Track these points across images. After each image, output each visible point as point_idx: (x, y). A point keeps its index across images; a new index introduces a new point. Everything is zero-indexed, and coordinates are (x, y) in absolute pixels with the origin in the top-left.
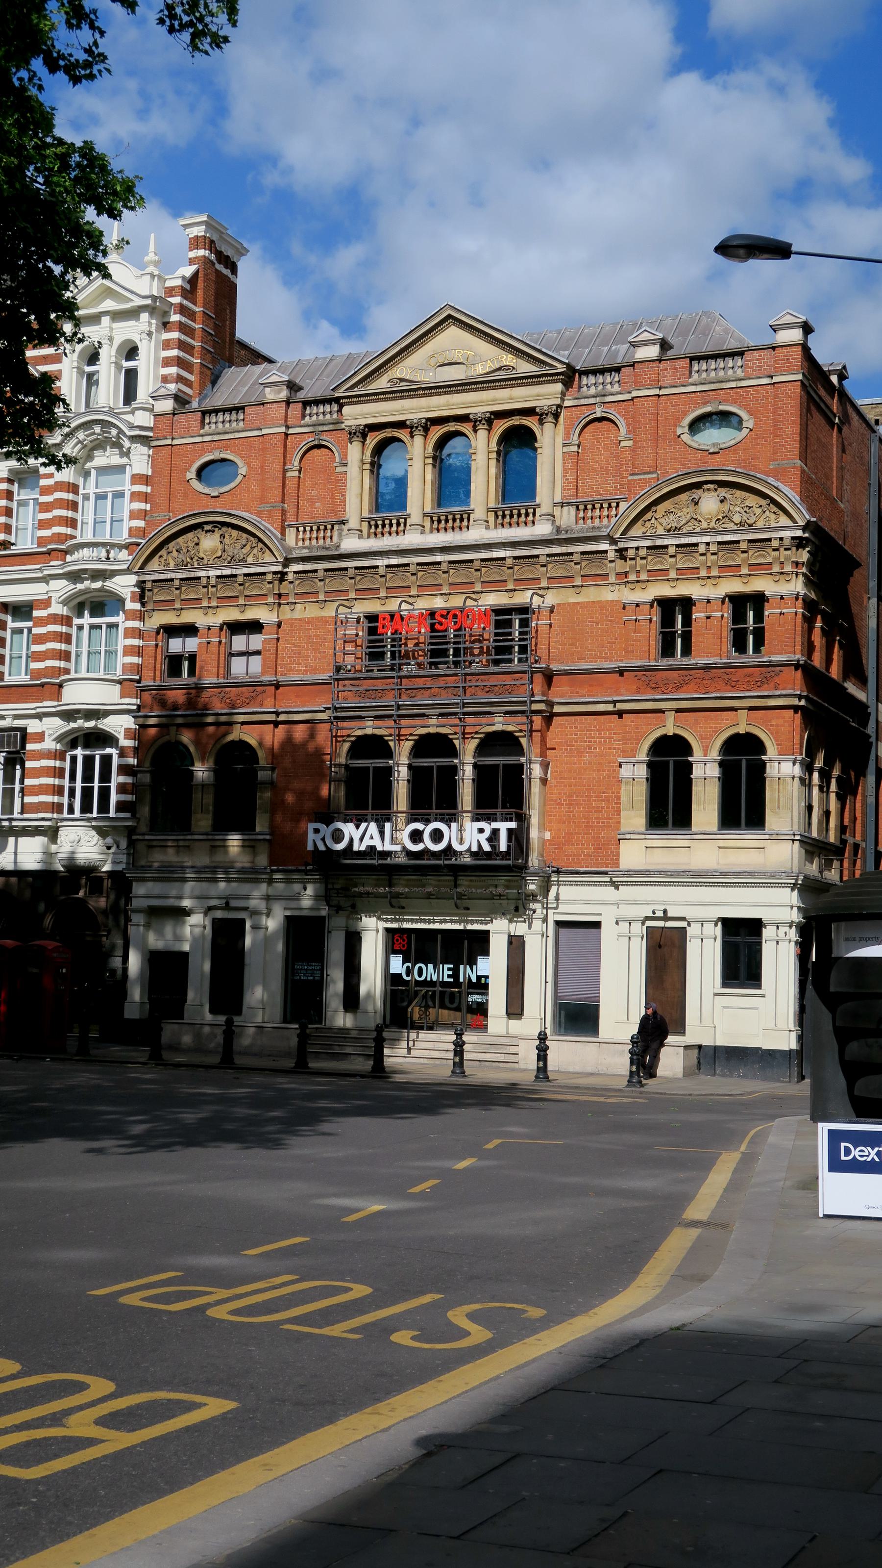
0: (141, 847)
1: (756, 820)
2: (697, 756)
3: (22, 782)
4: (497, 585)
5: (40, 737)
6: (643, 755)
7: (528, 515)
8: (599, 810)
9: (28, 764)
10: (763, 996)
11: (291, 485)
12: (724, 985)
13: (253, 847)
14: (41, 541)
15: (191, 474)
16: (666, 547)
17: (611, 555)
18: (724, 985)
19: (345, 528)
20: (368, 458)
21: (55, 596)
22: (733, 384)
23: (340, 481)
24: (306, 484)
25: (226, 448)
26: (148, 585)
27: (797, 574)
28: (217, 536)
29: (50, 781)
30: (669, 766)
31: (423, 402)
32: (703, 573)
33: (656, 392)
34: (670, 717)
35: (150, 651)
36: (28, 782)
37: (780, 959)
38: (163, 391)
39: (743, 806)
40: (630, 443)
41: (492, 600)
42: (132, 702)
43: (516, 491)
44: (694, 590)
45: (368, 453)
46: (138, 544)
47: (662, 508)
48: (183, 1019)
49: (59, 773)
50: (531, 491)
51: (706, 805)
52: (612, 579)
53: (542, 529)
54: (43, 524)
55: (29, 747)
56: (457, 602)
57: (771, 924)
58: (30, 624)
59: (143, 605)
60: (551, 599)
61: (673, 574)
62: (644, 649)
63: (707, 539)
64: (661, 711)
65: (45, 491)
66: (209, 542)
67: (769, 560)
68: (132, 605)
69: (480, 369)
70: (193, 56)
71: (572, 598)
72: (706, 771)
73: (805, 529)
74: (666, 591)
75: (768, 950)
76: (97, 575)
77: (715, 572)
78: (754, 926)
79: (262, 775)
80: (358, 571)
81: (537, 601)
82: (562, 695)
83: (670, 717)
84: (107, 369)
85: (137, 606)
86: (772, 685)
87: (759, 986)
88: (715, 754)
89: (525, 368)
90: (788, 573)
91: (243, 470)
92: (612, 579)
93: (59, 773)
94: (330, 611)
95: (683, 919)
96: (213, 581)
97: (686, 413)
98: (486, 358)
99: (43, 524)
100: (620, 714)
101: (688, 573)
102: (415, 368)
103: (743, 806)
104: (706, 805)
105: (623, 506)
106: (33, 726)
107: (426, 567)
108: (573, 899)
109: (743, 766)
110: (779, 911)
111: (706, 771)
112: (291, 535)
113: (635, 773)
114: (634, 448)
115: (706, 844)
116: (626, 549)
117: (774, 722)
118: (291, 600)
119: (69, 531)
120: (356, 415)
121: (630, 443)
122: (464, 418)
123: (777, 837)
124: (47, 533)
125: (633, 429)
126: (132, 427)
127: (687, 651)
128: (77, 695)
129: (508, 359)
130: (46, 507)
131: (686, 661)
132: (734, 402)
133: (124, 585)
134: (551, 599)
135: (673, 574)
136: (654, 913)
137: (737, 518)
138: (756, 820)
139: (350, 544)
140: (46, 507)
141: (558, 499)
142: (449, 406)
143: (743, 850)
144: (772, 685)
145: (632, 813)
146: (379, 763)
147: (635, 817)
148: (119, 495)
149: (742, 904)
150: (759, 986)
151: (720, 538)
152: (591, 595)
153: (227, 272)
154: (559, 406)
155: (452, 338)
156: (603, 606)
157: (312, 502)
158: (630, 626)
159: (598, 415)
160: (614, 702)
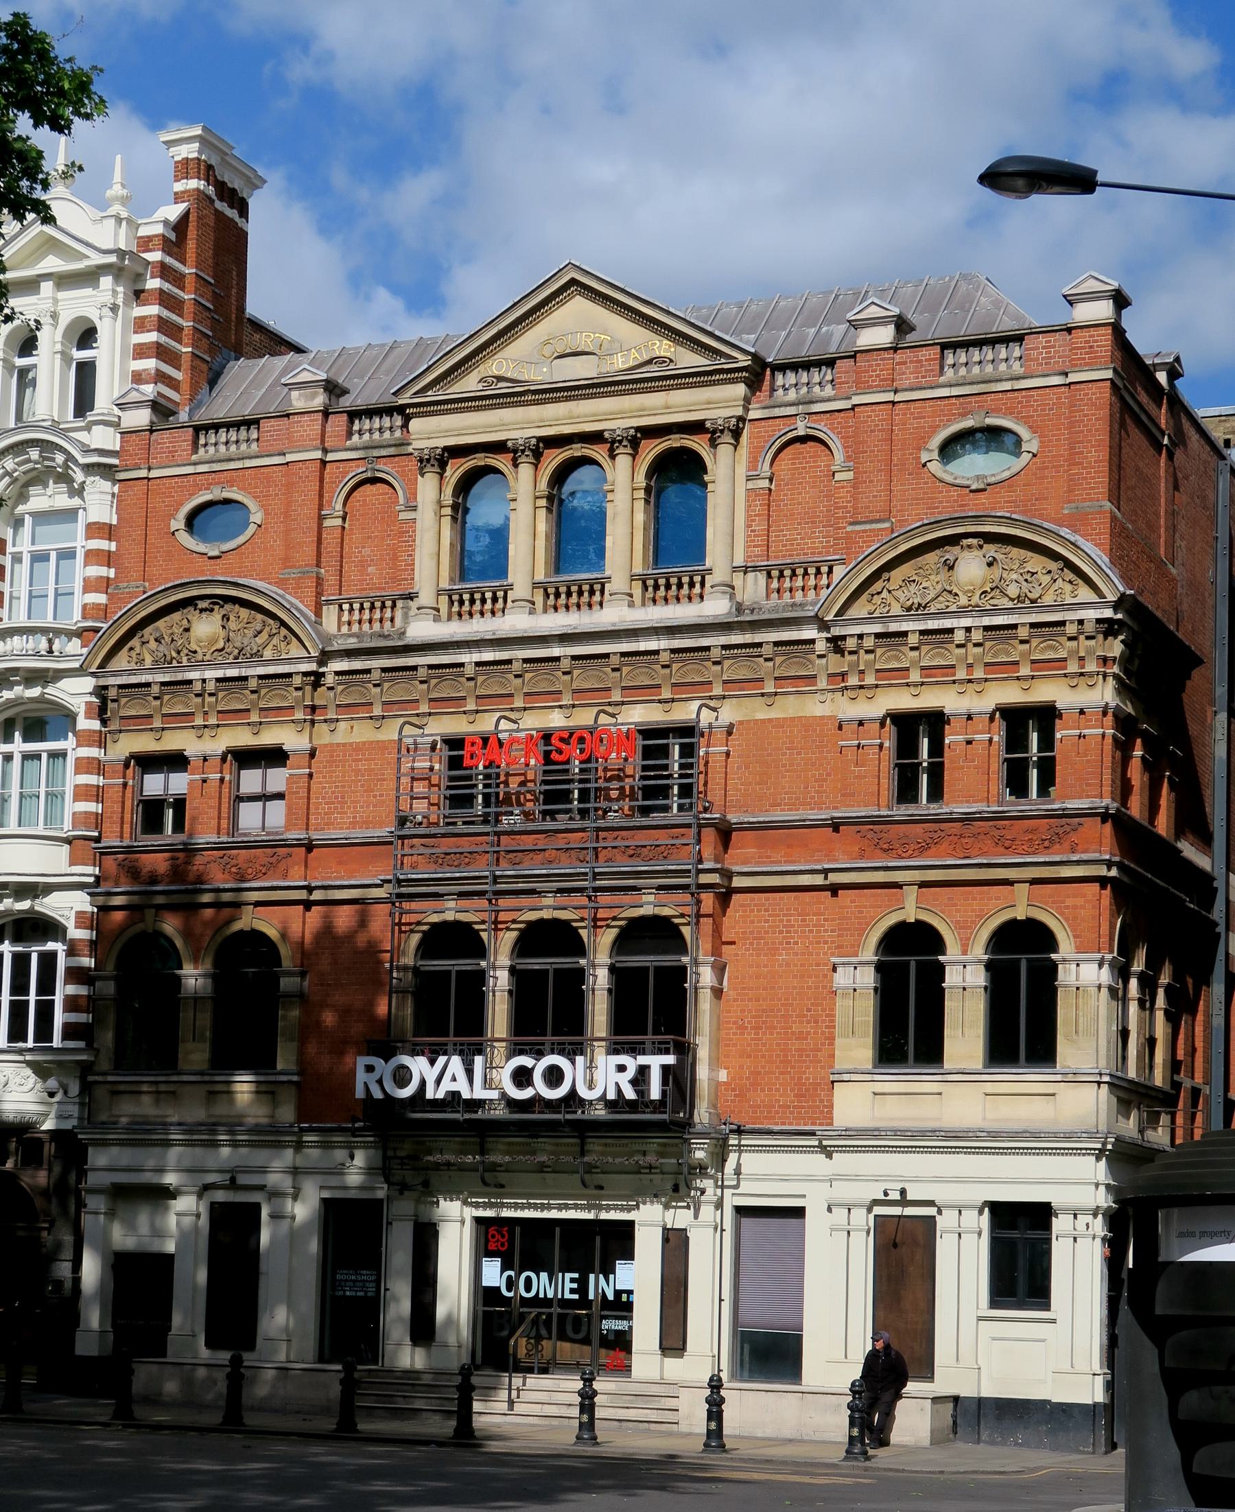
0: (100, 1093)
1: (1042, 1051)
2: (952, 953)
6: (869, 953)
8: (801, 1037)
10: (1053, 1321)
11: (330, 540)
12: (994, 1304)
13: (272, 1093)
15: (178, 523)
16: (904, 634)
17: (821, 646)
18: (994, 1304)
19: (413, 605)
22: (1007, 386)
23: (406, 533)
25: (231, 483)
26: (112, 693)
27: (1105, 676)
30: (909, 964)
31: (533, 412)
32: (961, 674)
33: (889, 397)
34: (911, 893)
35: (114, 794)
37: (1079, 1265)
38: (134, 397)
39: (1023, 1030)
40: (850, 475)
41: (639, 715)
43: (676, 548)
46: (96, 630)
48: (165, 1356)
52: (822, 683)
53: (715, 607)
57: (1066, 1211)
59: (104, 722)
60: (728, 713)
61: (915, 676)
62: (871, 792)
63: (967, 622)
66: (205, 627)
67: (1062, 654)
68: (87, 724)
69: (620, 362)
71: (759, 711)
72: (965, 978)
73: (1116, 606)
75: (1060, 1251)
77: (979, 673)
78: (1040, 1214)
79: (286, 983)
82: (745, 860)
83: (911, 893)
85: (96, 725)
86: (1066, 845)
87: (1047, 1307)
88: (979, 951)
89: (689, 360)
90: (1090, 674)
91: (257, 517)
92: (822, 683)
94: (390, 732)
95: (930, 1203)
96: (211, 686)
97: (934, 429)
98: (630, 345)
100: (834, 889)
101: (938, 675)
102: (520, 360)
103: (1023, 1030)
105: (839, 571)
107: (536, 664)
108: (763, 1173)
109: (1023, 963)
110: (1077, 1189)
111: (965, 978)
113: (857, 980)
114: (855, 483)
115: (965, 1088)
117: (1069, 902)
120: (430, 432)
121: (850, 475)
122: (595, 438)
123: (1074, 1078)
125: (854, 454)
126: (87, 451)
127: (936, 793)
129: (663, 347)
131: (934, 809)
132: (1009, 412)
133: (75, 693)
134: (728, 713)
135: (915, 676)
136: (886, 1194)
137: (1013, 591)
138: (1042, 1051)
139: (421, 629)
141: (739, 560)
143: (1022, 1097)
144: (1066, 845)
145: (853, 1041)
146: (465, 964)
147: (856, 1047)
148: (67, 555)
149: (1021, 1180)
150: (1047, 1307)
151: (987, 621)
152: (790, 707)
153: (232, 213)
154: (741, 419)
156: (808, 724)
157: (363, 565)
158: (850, 755)
159: (801, 432)
160: (826, 872)
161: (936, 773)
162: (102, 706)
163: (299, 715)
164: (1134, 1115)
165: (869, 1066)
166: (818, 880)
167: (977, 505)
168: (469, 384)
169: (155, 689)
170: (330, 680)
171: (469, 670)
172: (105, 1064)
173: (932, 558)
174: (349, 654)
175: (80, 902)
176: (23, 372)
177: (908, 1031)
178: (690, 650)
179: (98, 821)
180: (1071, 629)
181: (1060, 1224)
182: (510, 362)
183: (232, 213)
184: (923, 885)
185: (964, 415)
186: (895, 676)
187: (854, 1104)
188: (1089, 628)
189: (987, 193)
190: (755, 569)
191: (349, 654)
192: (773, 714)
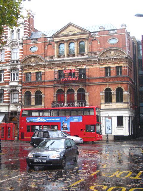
2: (112, 91)
3: (3, 98)
4: (80, 65)
5: (6, 91)
7: (84, 55)
8: (97, 100)
9: (4, 95)
10: (124, 128)
12: (118, 126)
14: (5, 60)
18: (118, 126)
19: (55, 57)
20: (78, 44)
21: (8, 69)
23: (53, 50)
24: (48, 50)
26: (23, 67)
28: (34, 59)
29: (8, 100)
30: (108, 93)
31: (67, 37)
36: (4, 98)
37: (126, 122)
38: (25, 36)
40: (100, 43)
41: (79, 68)
42: (20, 85)
44: (111, 66)
45: (58, 45)
46: (21, 60)
47: (105, 53)
49: (9, 99)
50: (84, 51)
51: (114, 100)
52: (98, 64)
53: (86, 57)
54: (5, 57)
55: (4, 92)
56: (74, 68)
57: (125, 116)
58: (3, 73)
59: (22, 69)
60: (88, 67)
61: (107, 63)
62: (103, 74)
64: (106, 84)
65: (5, 52)
66: (33, 60)
68: (20, 70)
69: (75, 32)
70: (22, 8)
72: (114, 93)
73: (128, 56)
74: (106, 66)
76: (14, 65)
80: (59, 64)
81: (86, 68)
83: (119, 85)
84: (15, 33)
85: (21, 70)
87: (123, 126)
89: (83, 32)
92: (98, 64)
93: (9, 75)
94: (53, 70)
95: (111, 116)
96: (34, 66)
99: (5, 57)
100: (100, 85)
101: (110, 63)
102: (64, 33)
103: (120, 99)
104: (114, 100)
105: (99, 53)
106: (5, 89)
107: (68, 64)
109: (119, 92)
111: (114, 93)
112: (46, 58)
113: (102, 94)
114: (100, 44)
116: (100, 59)
118: (46, 68)
119: (10, 58)
120: (56, 39)
121: (100, 43)
122: (63, 41)
124: (6, 59)
126: (20, 42)
127: (110, 75)
128: (12, 84)
129: (80, 31)
130: (6, 55)
133: (19, 67)
134: (88, 67)
135: (107, 63)
137: (117, 55)
139: (56, 59)
140: (6, 55)
142: (62, 39)
143: (120, 105)
145: (102, 100)
147: (103, 101)
148: (17, 52)
149: (120, 113)
150: (123, 126)
151: (114, 58)
152: (94, 67)
153: (33, 18)
154: (88, 38)
155: (71, 27)
156: (96, 68)
158: (101, 71)
159: (94, 39)
160: (99, 83)
161: (110, 72)
162: (21, 68)
163: (43, 68)
164: (55, 128)
165: (115, 102)
166: (98, 84)
167: (112, 46)
168: (60, 35)
169: (28, 66)
170: (46, 65)
171: (87, 61)
172: (24, 104)
173: (109, 51)
174: (48, 62)
175: (20, 88)
176: (18, 33)
177: (108, 100)
178: (84, 62)
179: (22, 80)
180: (123, 59)
181: (124, 118)
182: (64, 33)
183: (33, 18)
184: (120, 84)
185: (111, 37)
186: (116, 63)
187: (103, 106)
188: (125, 58)
189: (135, 17)
190: (91, 53)
191: (48, 62)
192: (93, 67)
